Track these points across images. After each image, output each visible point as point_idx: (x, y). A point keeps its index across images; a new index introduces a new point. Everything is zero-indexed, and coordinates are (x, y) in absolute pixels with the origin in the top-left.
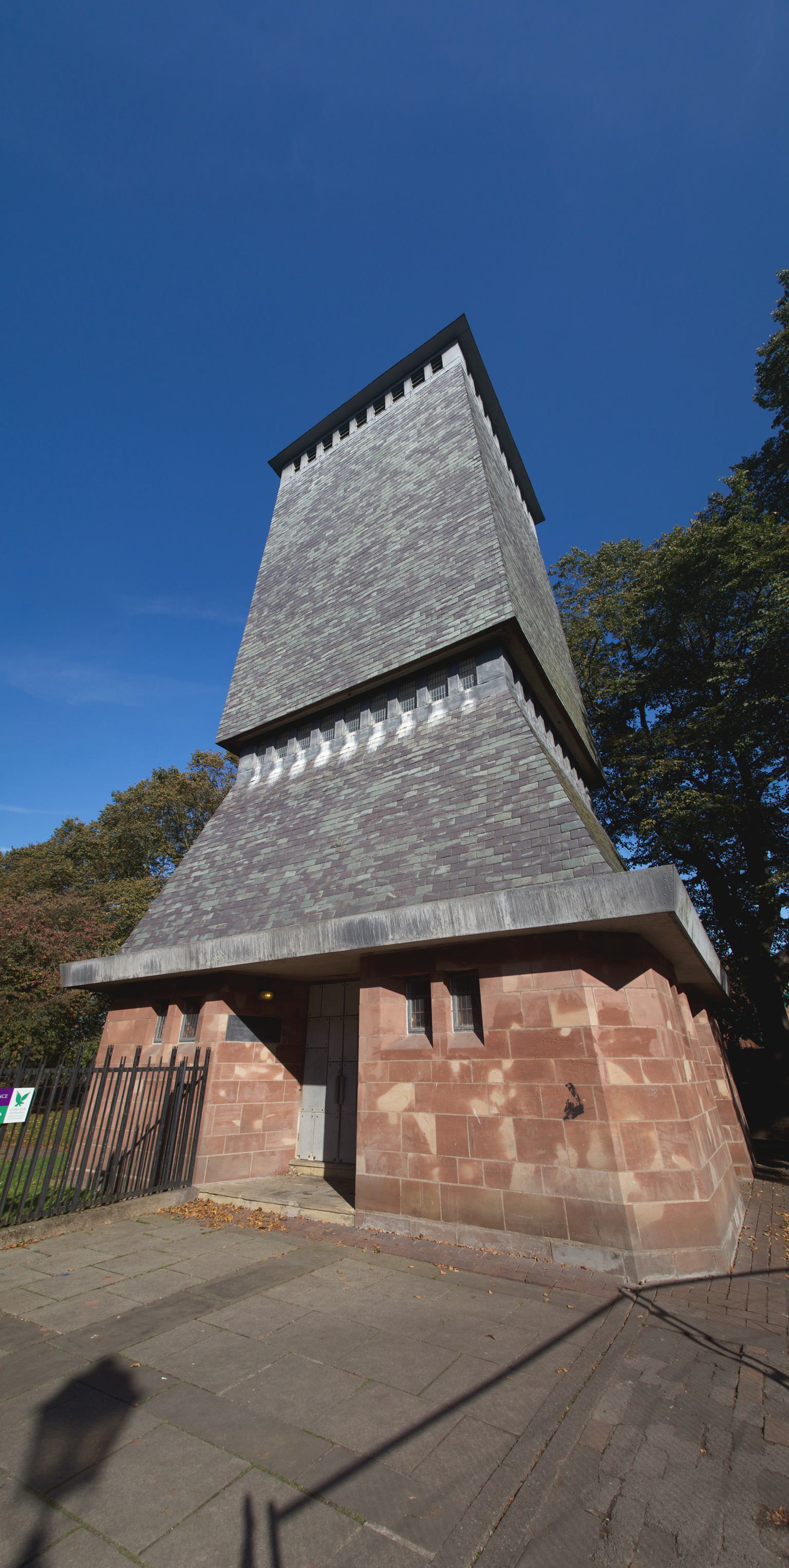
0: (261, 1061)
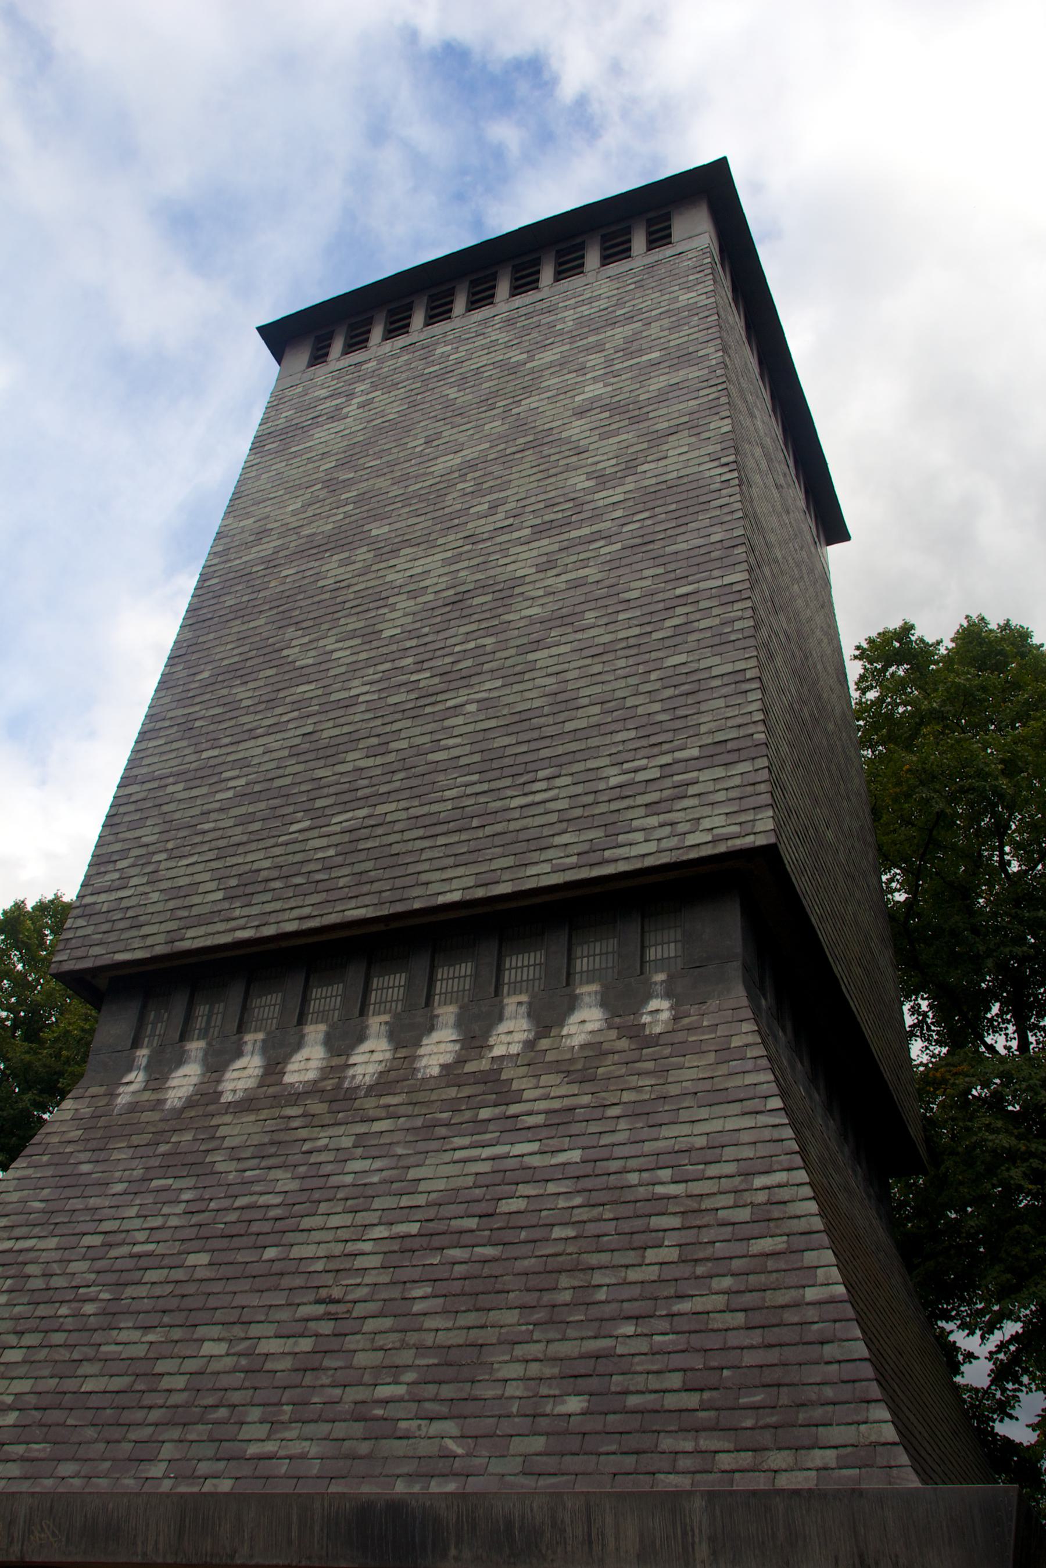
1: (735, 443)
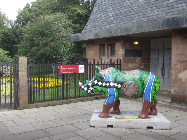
0: (136, 63)
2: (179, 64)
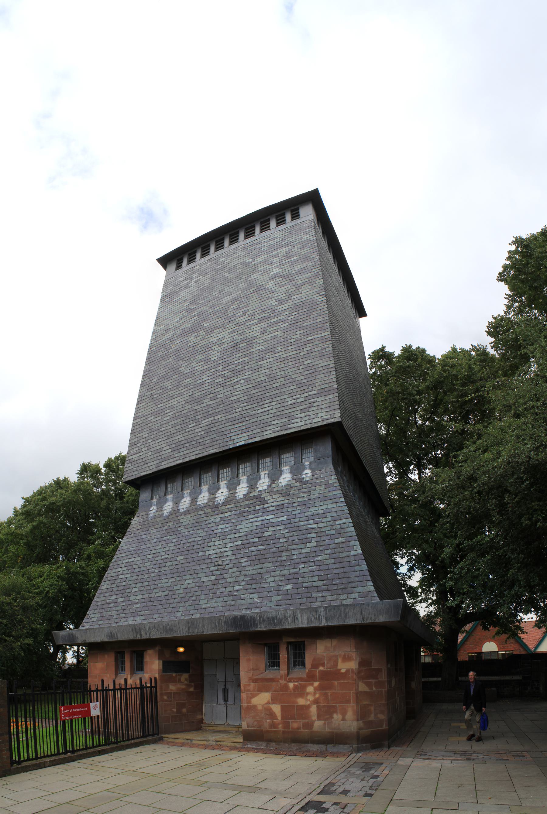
1: (326, 287)
2: (252, 684)
